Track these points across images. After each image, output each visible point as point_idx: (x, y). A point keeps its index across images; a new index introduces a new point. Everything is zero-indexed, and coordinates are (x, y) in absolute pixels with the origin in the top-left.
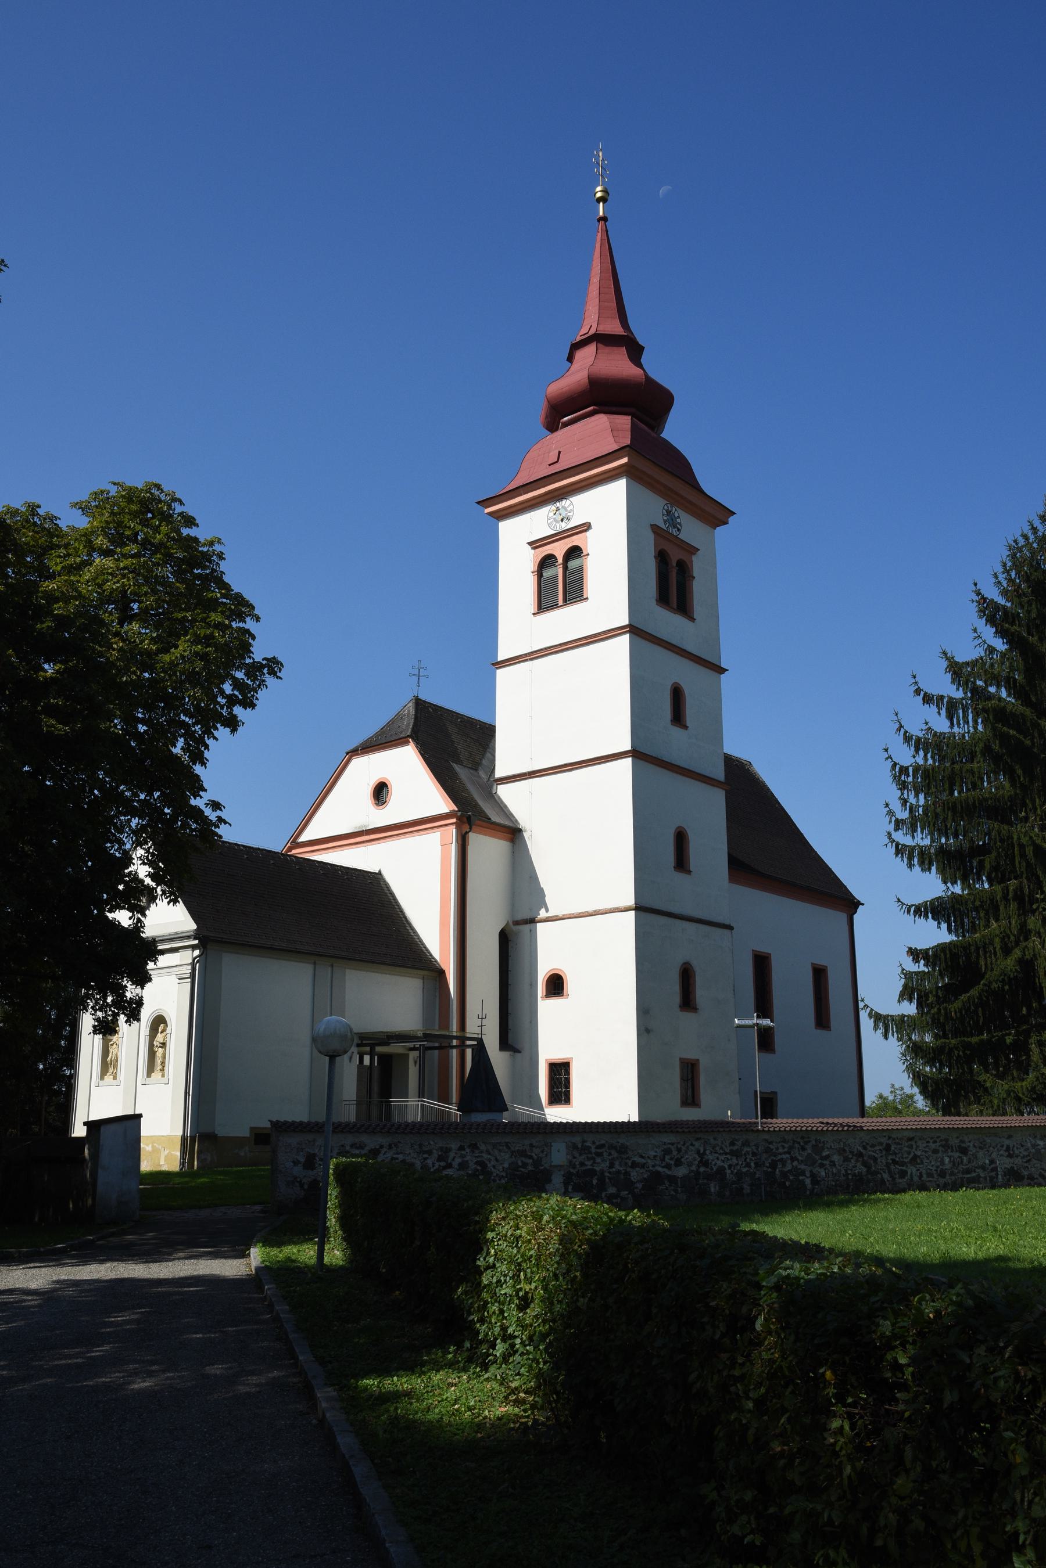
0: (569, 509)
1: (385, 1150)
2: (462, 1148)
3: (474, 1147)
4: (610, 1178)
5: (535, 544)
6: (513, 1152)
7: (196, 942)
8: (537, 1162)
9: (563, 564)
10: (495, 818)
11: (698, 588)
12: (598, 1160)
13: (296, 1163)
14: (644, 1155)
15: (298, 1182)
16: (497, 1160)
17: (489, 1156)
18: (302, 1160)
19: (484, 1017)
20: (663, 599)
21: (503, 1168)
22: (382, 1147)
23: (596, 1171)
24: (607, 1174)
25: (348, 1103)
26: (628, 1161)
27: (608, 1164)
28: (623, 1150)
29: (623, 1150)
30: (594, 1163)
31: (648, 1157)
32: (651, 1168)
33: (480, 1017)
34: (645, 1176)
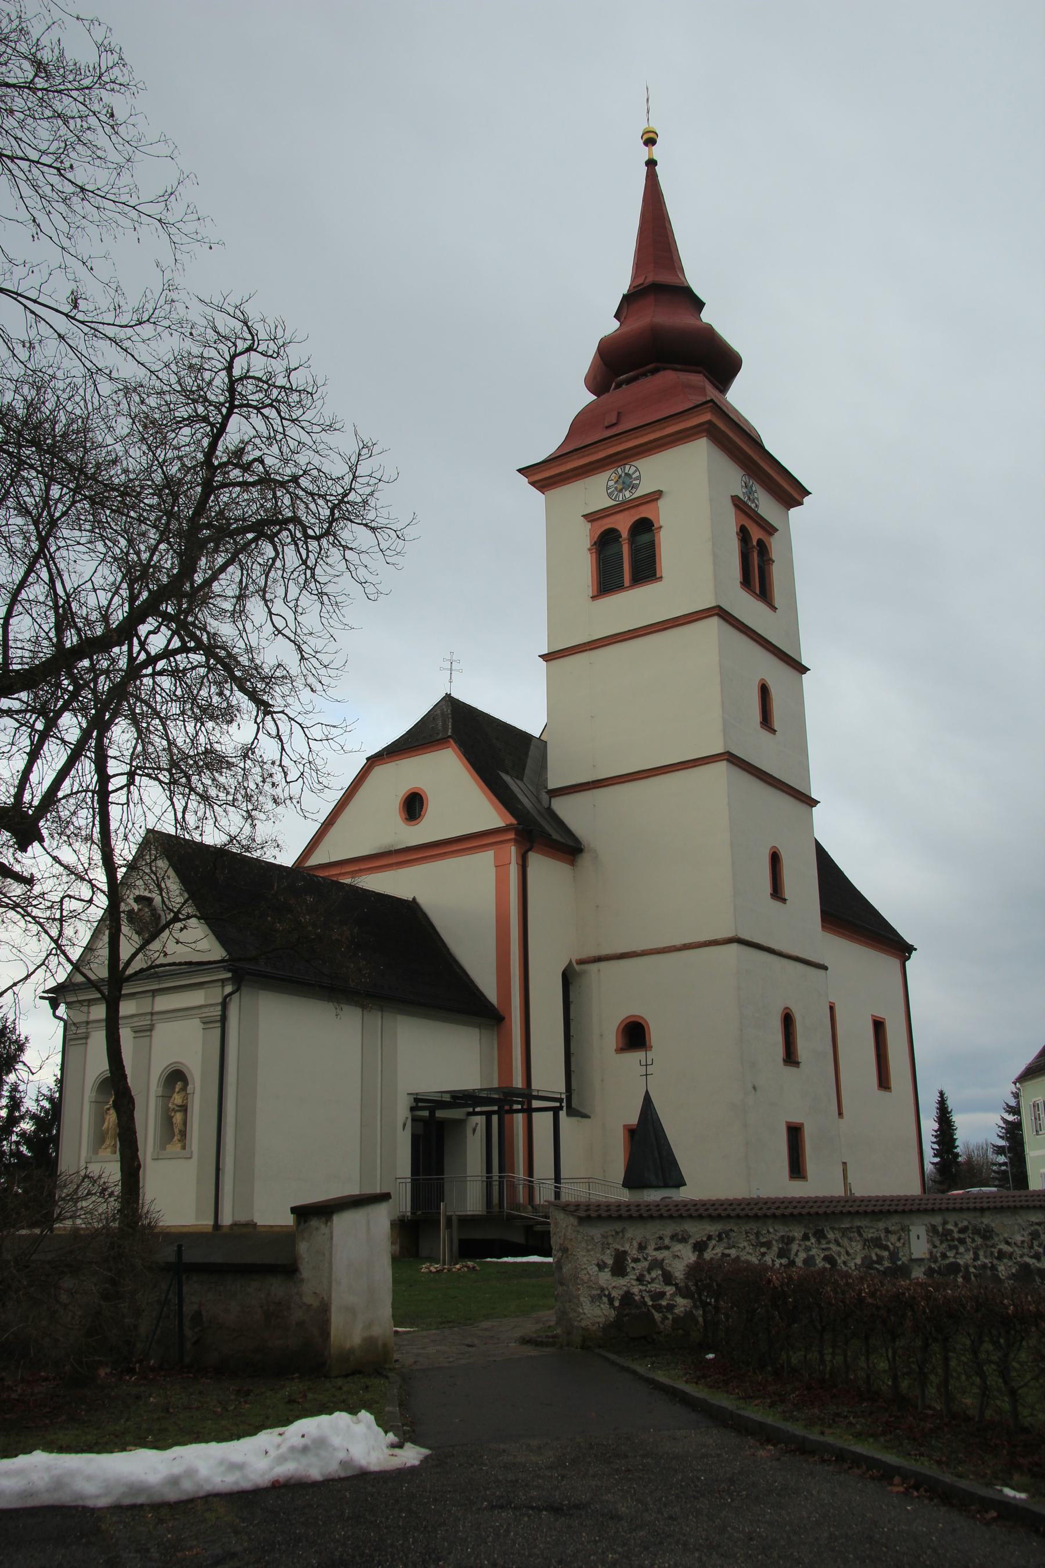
0: (634, 476)
1: (714, 1242)
2: (806, 1237)
3: (820, 1235)
4: (976, 1276)
5: (591, 518)
6: (866, 1240)
7: (229, 975)
8: (894, 1256)
9: (629, 539)
10: (555, 836)
11: (776, 571)
12: (962, 1249)
13: (601, 1266)
14: (1010, 1240)
15: (605, 1295)
16: (848, 1253)
17: (839, 1248)
18: (610, 1262)
19: (649, 1062)
20: (746, 582)
21: (856, 1264)
22: (710, 1238)
23: (958, 1265)
24: (972, 1270)
25: (403, 1180)
26: (993, 1250)
27: (971, 1254)
28: (988, 1234)
29: (988, 1234)
30: (957, 1253)
31: (1015, 1244)
32: (1019, 1259)
33: (643, 1063)
34: (1014, 1271)
